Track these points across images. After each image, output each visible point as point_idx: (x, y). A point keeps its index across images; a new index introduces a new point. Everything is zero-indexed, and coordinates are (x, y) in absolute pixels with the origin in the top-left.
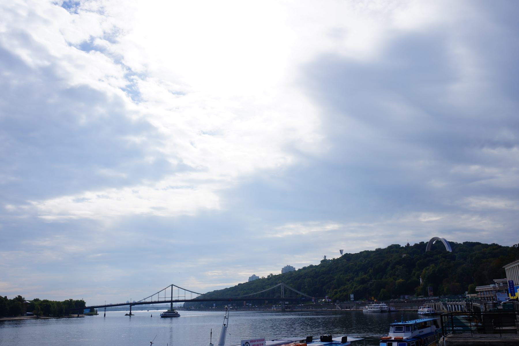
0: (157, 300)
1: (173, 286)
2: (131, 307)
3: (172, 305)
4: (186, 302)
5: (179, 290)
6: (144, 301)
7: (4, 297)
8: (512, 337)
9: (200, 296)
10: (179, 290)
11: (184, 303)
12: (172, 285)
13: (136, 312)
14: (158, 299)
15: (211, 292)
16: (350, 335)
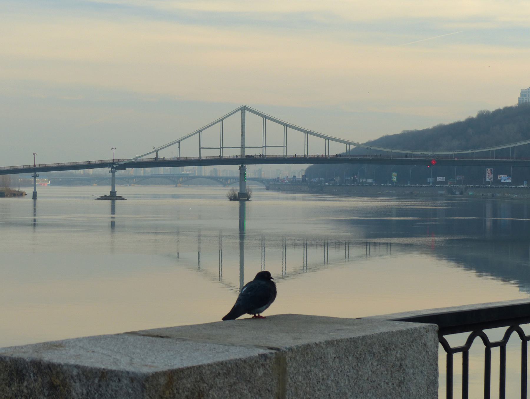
1: (247, 112)
2: (113, 172)
5: (264, 125)
9: (354, 149)
10: (264, 125)
11: (305, 166)
12: (244, 109)
13: (379, 218)
14: (200, 152)
15: (395, 136)
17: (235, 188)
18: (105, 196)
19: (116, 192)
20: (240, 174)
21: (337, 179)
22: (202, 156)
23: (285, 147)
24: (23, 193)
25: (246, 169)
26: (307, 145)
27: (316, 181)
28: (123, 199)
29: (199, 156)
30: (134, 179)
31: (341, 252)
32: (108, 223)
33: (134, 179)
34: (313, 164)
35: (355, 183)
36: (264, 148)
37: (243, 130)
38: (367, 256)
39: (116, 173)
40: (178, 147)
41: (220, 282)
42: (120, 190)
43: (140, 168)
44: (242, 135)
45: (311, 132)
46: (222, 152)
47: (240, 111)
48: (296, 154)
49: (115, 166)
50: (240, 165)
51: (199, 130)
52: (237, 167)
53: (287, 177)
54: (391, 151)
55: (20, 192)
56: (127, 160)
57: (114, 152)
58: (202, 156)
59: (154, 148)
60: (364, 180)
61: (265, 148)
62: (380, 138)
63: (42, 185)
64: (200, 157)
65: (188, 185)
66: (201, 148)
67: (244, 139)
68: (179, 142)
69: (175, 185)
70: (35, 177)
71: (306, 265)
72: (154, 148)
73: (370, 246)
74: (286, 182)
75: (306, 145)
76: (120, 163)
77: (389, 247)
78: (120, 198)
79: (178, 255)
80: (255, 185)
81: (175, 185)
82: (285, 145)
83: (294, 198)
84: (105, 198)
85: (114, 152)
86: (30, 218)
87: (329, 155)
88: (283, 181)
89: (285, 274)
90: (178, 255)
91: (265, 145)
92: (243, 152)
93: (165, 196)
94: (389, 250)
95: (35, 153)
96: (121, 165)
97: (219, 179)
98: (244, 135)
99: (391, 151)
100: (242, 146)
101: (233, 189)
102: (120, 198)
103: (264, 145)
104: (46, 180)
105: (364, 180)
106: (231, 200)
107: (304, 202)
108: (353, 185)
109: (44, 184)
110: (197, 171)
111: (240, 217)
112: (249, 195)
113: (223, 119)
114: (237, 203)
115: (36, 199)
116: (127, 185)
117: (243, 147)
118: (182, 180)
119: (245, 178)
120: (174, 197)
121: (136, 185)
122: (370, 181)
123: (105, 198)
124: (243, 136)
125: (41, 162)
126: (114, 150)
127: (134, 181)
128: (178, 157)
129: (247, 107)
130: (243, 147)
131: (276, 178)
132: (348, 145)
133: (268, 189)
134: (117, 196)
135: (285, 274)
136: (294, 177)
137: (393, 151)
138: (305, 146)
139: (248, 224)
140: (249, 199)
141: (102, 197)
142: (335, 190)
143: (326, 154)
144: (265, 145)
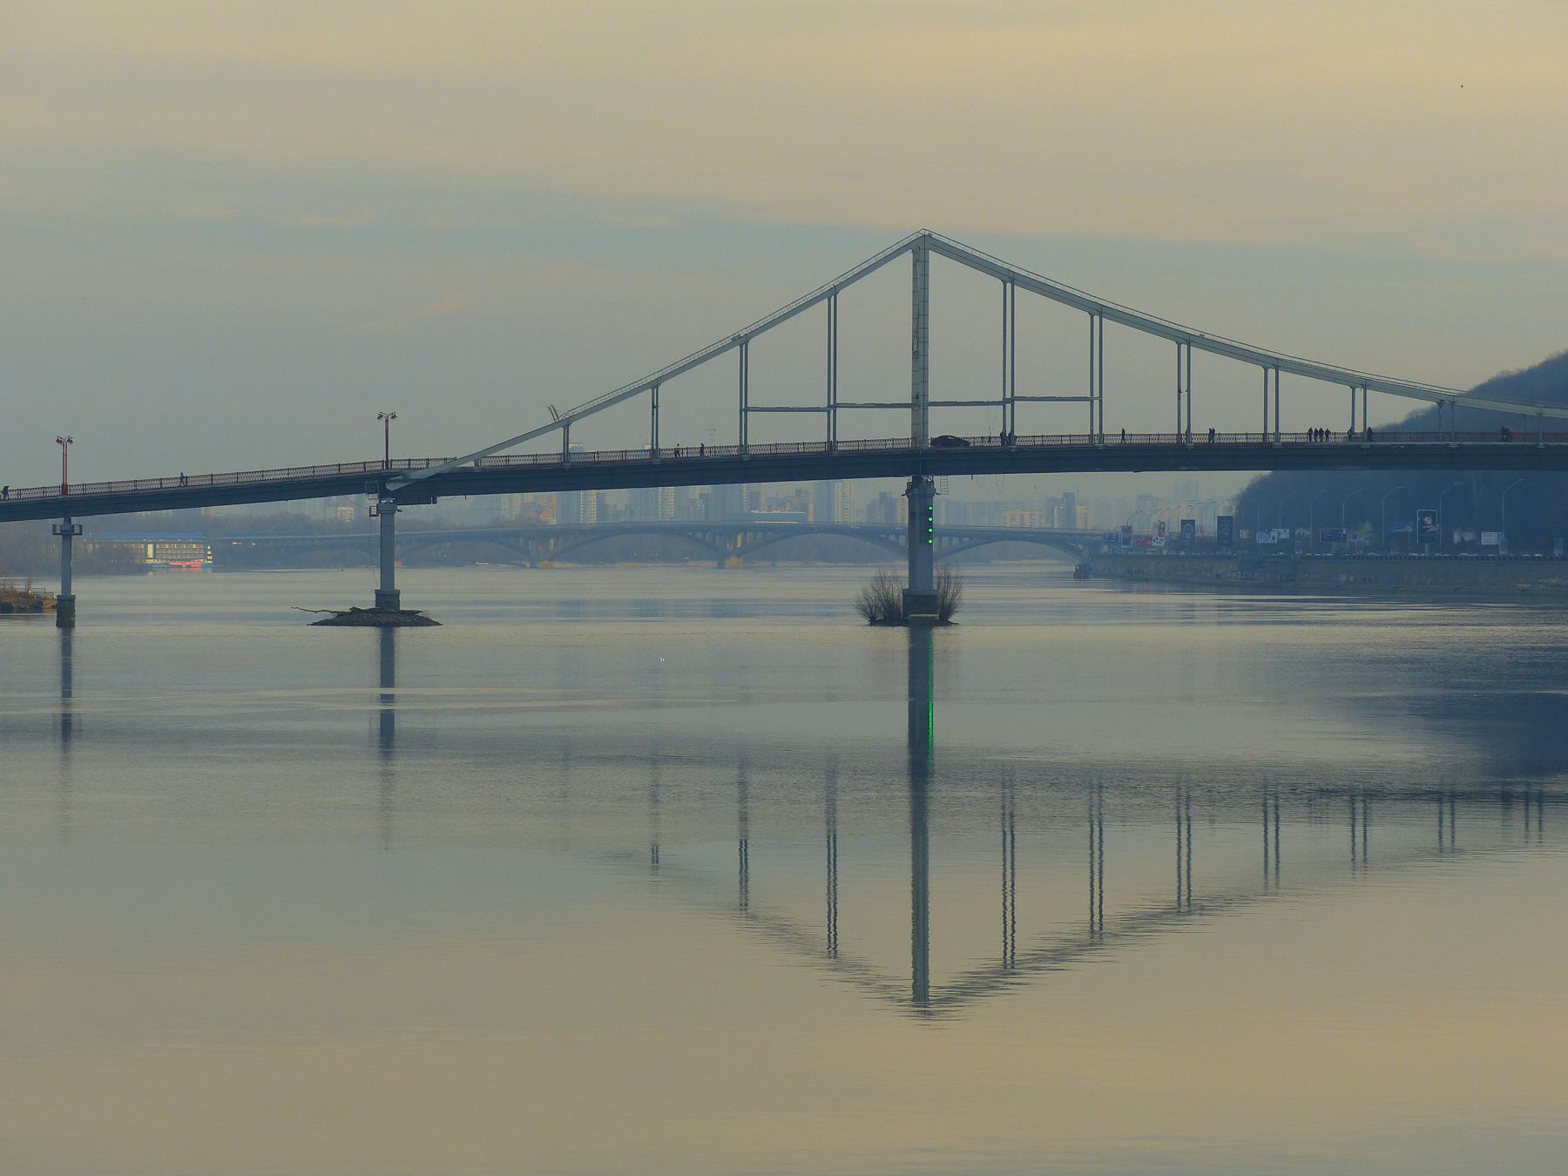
0: (722, 436)
1: (934, 258)
2: (386, 513)
3: (920, 500)
4: (1283, 474)
6: (548, 447)
7: (438, 498)
8: (1538, 606)
11: (1242, 479)
12: (923, 247)
16: (869, 564)
17: (889, 574)
18: (355, 611)
19: (397, 594)
20: (912, 514)
21: (1362, 535)
22: (1016, 434)
23: (1096, 402)
24: (45, 599)
25: (934, 492)
26: (1188, 391)
27: (1270, 541)
28: (427, 622)
29: (741, 441)
30: (552, 541)
31: (1336, 835)
32: (367, 726)
33: (552, 541)
34: (1268, 473)
35: (1427, 547)
36: (1008, 406)
37: (921, 335)
38: (1444, 851)
39: (397, 514)
40: (653, 407)
41: (828, 961)
42: (413, 588)
43: (582, 492)
44: (915, 354)
45: (1202, 337)
46: (832, 426)
47: (908, 257)
48: (1123, 431)
49: (391, 487)
50: (909, 479)
51: (739, 337)
52: (898, 485)
53: (1161, 528)
54: (1540, 415)
55: (32, 597)
56: (442, 463)
57: (65, 455)
58: (749, 443)
59: (553, 410)
60: (1468, 537)
61: (835, 411)
62: (1544, 362)
63: (180, 566)
64: (831, 444)
65: (770, 563)
66: (745, 410)
67: (925, 368)
68: (655, 385)
69: (716, 564)
70: (67, 534)
71: (1189, 893)
72: (553, 410)
73: (1540, 811)
74: (1154, 544)
75: (1184, 391)
76: (415, 475)
77: (1534, 809)
78: (417, 619)
79: (655, 850)
80: (1050, 561)
81: (716, 564)
82: (1096, 394)
83: (1187, 616)
84: (352, 618)
85: (65, 455)
86: (49, 709)
87: (1277, 434)
88: (1145, 541)
89: (1101, 929)
90: (655, 850)
91: (1013, 394)
92: (920, 423)
93: (682, 610)
94: (1534, 825)
95: (64, 436)
96: (419, 482)
97: (892, 538)
98: (925, 355)
99: (1540, 415)
100: (918, 398)
101: (881, 578)
102: (417, 619)
103: (1008, 396)
104: (194, 546)
105: (1468, 537)
106: (873, 621)
107: (1228, 628)
108: (1437, 555)
109: (188, 564)
110: (811, 506)
111: (912, 693)
112: (948, 601)
113: (834, 291)
114: (898, 636)
115: (72, 625)
116: (524, 566)
117: (919, 404)
118: (744, 542)
119: (930, 530)
120: (722, 610)
121: (557, 564)
122: (1490, 538)
123: (352, 618)
124: (921, 358)
125: (89, 473)
126: (65, 447)
127: (552, 547)
128: (829, 442)
129: (934, 236)
130: (919, 404)
131: (1119, 530)
132: (1357, 390)
133: (1081, 575)
134: (404, 612)
135: (1101, 929)
136: (1188, 524)
137: (1549, 412)
138: (1179, 399)
139: (946, 726)
140: (950, 620)
141: (341, 614)
142: (1343, 578)
143: (1266, 428)
144: (1013, 394)
